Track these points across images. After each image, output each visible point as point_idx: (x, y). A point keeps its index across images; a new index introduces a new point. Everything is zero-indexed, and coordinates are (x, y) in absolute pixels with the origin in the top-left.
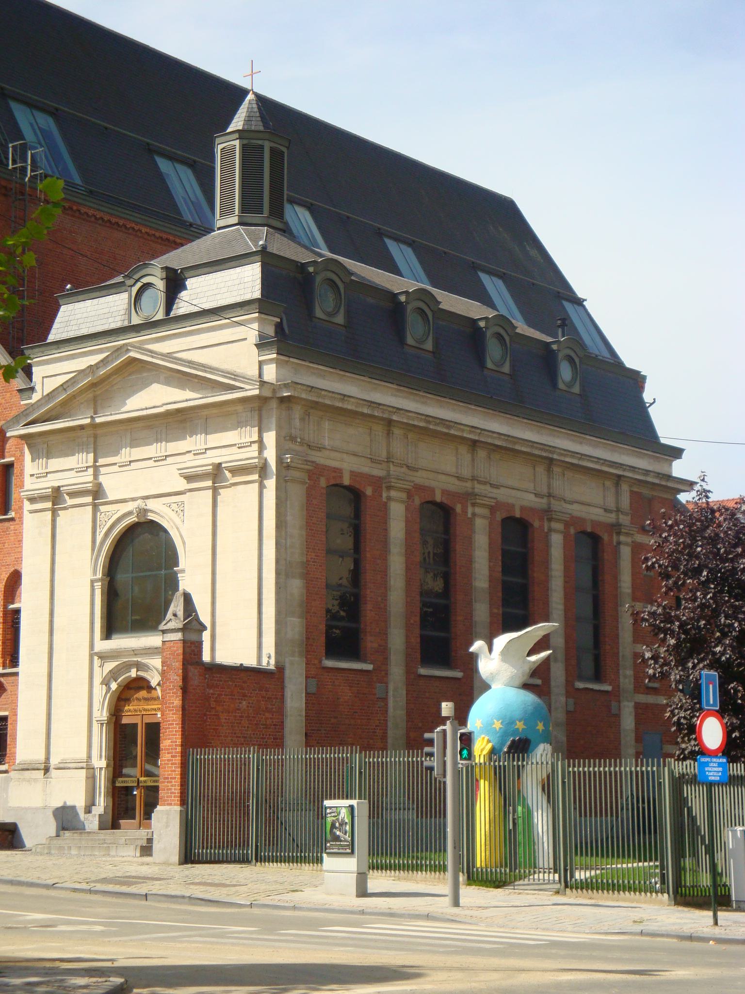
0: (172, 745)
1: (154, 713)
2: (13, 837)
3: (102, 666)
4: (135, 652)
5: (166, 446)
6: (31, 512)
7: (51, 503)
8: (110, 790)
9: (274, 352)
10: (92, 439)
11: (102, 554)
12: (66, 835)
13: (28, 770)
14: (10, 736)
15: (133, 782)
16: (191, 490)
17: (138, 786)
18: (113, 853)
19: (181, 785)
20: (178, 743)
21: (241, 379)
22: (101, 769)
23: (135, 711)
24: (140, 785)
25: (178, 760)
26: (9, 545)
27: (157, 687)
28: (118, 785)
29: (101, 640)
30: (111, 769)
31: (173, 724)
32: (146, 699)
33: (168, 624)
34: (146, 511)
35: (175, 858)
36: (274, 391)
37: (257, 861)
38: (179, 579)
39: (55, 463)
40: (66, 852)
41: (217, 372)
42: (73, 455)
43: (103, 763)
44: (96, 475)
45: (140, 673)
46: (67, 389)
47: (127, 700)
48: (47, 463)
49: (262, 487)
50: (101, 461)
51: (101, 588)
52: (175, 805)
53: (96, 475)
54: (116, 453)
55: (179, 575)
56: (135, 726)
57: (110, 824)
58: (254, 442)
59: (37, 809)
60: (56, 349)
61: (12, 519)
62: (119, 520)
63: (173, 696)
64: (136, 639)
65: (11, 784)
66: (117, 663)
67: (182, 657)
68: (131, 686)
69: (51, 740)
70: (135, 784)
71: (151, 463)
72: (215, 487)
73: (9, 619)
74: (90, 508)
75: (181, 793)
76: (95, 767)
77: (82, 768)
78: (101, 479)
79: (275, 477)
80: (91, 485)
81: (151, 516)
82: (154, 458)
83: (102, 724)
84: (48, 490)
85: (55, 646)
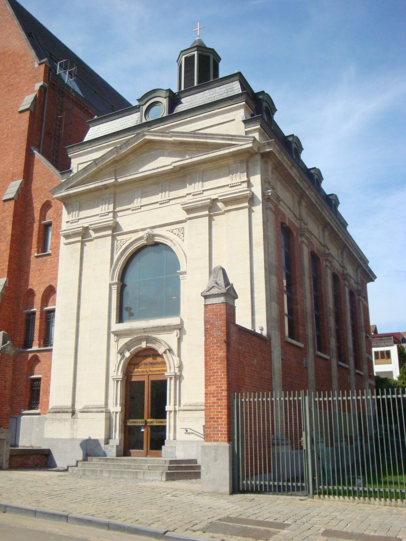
0: (218, 390)
1: (162, 373)
2: (47, 460)
3: (117, 341)
4: (145, 330)
5: (169, 194)
6: (66, 244)
7: (81, 237)
8: (123, 428)
9: (258, 124)
10: (113, 195)
11: (118, 267)
12: (94, 460)
13: (59, 412)
14: (42, 390)
15: (142, 422)
16: (190, 219)
17: (145, 426)
18: (140, 477)
19: (228, 424)
20: (223, 388)
21: (237, 138)
22: (116, 413)
23: (143, 372)
24: (148, 424)
25: (224, 402)
26: (46, 270)
27: (164, 354)
28: (129, 424)
29: (116, 323)
30: (123, 413)
31: (218, 372)
32: (151, 364)
33: (211, 291)
34: (154, 236)
35: (226, 488)
36: (259, 149)
37: (314, 494)
38: (181, 279)
39: (84, 213)
40: (98, 474)
41: (217, 137)
42: (98, 206)
43: (119, 409)
44: (115, 216)
45: (150, 345)
46: (98, 164)
47: (137, 365)
48: (79, 214)
49: (250, 212)
50: (118, 209)
51: (117, 289)
52: (222, 441)
53: (115, 216)
54: (132, 201)
55: (180, 276)
56: (142, 383)
57: (123, 454)
58: (244, 182)
59: (66, 440)
60: (89, 146)
61: (49, 255)
62: (132, 244)
63: (217, 349)
64: (146, 321)
65: (47, 422)
66: (130, 339)
67: (225, 316)
68: (139, 355)
69: (76, 392)
70: (144, 424)
71: (157, 205)
72: (210, 215)
73: (44, 317)
74: (110, 238)
75: (228, 431)
76: (111, 411)
77: (102, 412)
78: (118, 220)
79: (261, 204)
80: (112, 222)
81: (157, 239)
82: (160, 202)
83: (117, 381)
84: (79, 229)
85: (208, 248)
